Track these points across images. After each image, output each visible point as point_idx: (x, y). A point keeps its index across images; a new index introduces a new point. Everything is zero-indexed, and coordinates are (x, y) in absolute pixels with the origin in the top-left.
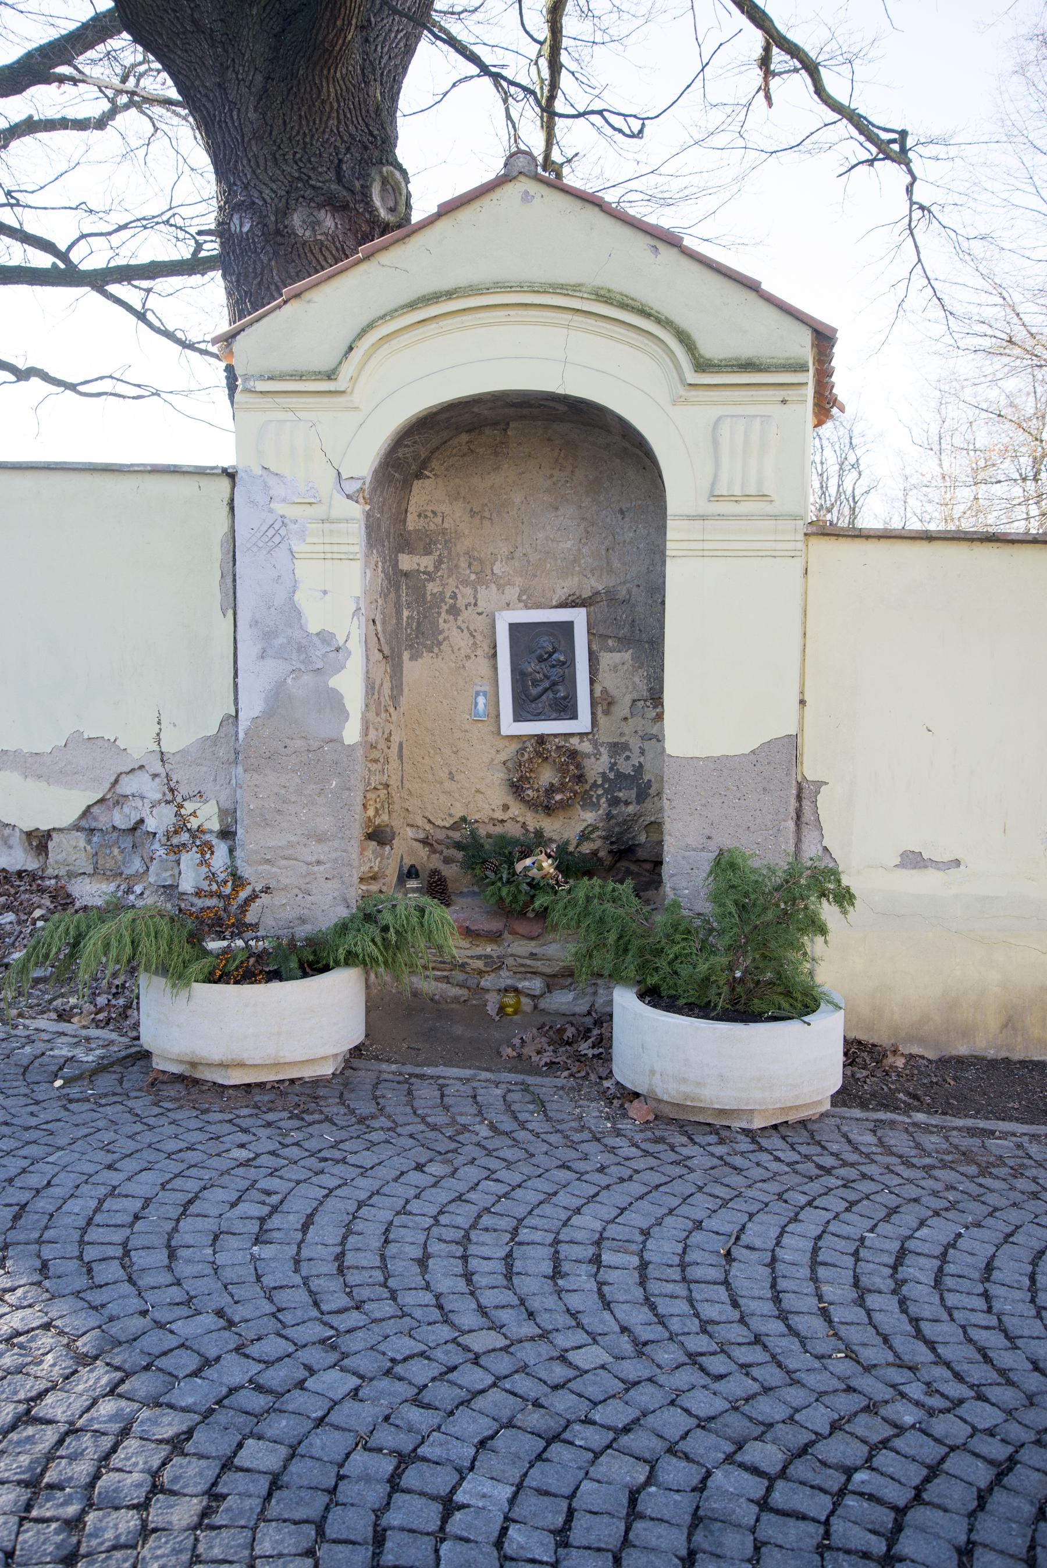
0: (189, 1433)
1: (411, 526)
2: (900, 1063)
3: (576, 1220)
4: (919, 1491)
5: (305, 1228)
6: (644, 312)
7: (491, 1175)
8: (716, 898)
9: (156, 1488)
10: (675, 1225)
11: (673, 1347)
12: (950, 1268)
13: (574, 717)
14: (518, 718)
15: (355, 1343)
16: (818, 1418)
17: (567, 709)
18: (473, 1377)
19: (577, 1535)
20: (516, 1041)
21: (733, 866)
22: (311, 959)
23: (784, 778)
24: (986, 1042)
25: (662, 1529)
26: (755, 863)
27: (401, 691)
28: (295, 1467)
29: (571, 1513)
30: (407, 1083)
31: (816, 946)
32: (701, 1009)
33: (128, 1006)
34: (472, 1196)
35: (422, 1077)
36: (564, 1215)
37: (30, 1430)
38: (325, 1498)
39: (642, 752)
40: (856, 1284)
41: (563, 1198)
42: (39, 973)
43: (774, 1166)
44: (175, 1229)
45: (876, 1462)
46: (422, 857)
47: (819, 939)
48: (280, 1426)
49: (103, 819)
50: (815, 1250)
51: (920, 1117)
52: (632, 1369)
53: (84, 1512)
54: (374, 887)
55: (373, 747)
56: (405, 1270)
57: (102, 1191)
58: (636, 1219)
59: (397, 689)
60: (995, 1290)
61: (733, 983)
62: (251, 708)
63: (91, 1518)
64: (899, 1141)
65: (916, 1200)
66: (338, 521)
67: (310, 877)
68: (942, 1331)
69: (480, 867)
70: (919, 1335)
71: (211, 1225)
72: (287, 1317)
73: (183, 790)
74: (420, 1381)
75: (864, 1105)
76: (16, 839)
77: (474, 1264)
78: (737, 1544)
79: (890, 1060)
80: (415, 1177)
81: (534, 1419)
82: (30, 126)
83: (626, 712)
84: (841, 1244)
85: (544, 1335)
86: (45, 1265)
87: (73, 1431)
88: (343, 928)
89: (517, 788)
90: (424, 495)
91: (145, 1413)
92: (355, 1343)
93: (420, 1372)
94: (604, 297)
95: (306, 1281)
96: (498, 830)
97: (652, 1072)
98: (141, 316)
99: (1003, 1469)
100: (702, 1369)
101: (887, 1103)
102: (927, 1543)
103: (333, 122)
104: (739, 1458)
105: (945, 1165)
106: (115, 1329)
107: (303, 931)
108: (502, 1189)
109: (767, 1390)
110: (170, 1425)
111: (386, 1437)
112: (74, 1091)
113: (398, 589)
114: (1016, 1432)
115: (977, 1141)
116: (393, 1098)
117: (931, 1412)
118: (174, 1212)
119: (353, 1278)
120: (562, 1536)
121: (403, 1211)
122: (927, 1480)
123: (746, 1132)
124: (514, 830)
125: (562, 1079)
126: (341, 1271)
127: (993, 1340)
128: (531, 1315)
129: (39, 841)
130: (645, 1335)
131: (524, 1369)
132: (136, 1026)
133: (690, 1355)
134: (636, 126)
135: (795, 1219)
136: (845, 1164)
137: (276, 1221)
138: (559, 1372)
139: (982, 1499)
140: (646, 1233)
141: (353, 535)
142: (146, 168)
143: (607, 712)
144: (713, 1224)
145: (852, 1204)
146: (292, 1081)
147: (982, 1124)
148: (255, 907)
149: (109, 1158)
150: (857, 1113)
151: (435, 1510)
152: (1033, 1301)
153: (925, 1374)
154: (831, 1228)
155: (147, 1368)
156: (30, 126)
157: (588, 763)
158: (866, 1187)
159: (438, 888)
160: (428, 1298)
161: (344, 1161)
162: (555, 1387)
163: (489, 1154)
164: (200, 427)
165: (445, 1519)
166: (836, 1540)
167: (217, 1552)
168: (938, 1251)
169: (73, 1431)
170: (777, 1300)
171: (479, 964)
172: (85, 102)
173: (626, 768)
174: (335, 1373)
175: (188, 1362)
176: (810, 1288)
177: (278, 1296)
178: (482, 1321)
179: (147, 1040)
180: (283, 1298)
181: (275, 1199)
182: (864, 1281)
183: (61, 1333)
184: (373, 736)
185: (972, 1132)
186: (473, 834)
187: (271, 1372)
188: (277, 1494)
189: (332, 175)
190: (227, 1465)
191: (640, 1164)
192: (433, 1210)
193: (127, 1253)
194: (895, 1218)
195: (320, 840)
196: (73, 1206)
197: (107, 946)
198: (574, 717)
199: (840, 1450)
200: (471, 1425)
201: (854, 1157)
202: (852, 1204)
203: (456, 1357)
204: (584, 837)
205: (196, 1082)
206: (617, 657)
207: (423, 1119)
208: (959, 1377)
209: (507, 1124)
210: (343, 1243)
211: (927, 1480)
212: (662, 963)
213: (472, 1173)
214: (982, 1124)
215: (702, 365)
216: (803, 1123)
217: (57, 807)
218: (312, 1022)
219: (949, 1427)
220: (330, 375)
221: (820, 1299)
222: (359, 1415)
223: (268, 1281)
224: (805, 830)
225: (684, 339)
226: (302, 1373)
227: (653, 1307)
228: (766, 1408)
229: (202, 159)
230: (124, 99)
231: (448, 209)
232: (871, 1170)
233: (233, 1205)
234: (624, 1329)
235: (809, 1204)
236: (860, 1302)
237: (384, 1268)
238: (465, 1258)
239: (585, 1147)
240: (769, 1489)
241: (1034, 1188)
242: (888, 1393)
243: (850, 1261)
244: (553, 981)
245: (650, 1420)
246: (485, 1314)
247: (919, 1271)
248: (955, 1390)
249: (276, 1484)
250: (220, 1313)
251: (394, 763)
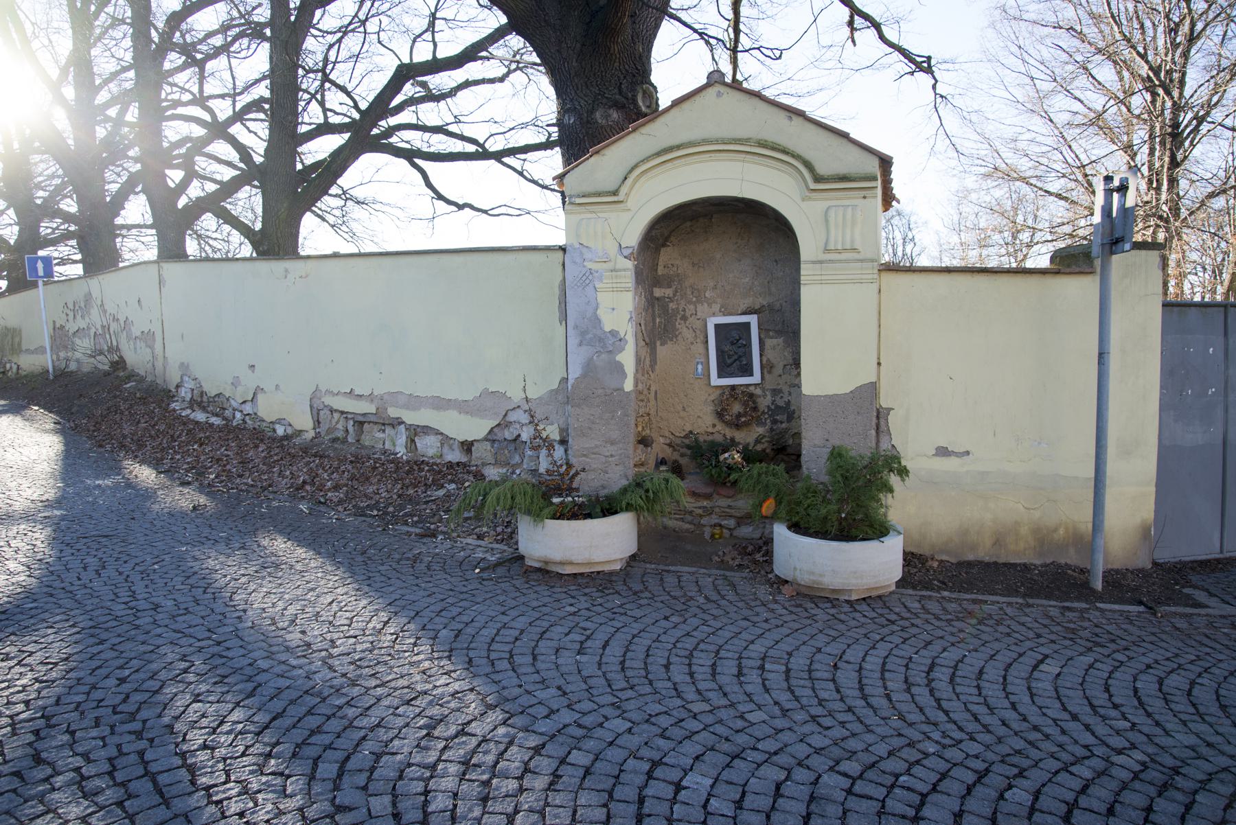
0: (543, 745)
1: (660, 273)
2: (935, 564)
3: (751, 647)
4: (935, 786)
5: (604, 647)
6: (785, 151)
7: (705, 623)
8: (830, 473)
9: (527, 770)
10: (806, 651)
11: (802, 712)
12: (959, 673)
13: (752, 375)
14: (720, 376)
15: (631, 705)
16: (882, 749)
17: (747, 371)
18: (694, 725)
19: (747, 803)
20: (721, 553)
21: (840, 455)
22: (606, 507)
23: (867, 404)
24: (984, 553)
25: (793, 803)
26: (853, 453)
27: (656, 363)
28: (598, 764)
29: (744, 793)
30: (660, 575)
31: (887, 499)
32: (822, 533)
33: (513, 532)
34: (694, 633)
35: (668, 571)
36: (745, 644)
37: (464, 739)
38: (614, 780)
39: (790, 394)
40: (906, 681)
41: (744, 635)
42: (466, 515)
43: (863, 620)
44: (536, 646)
45: (912, 771)
46: (668, 453)
47: (890, 495)
48: (590, 744)
49: (499, 435)
50: (884, 664)
51: (946, 594)
52: (779, 723)
53: (491, 779)
54: (642, 470)
55: (641, 393)
56: (657, 670)
57: (499, 625)
58: (785, 646)
59: (654, 361)
60: (983, 684)
61: (840, 520)
62: (575, 373)
63: (495, 781)
64: (933, 607)
65: (942, 638)
66: (620, 270)
67: (607, 462)
68: (954, 706)
69: (701, 458)
70: (940, 707)
71: (555, 644)
72: (594, 692)
73: (538, 416)
74: (664, 726)
75: (914, 588)
76: (456, 446)
77: (694, 668)
78: (834, 810)
79: (930, 563)
80: (664, 623)
81: (726, 747)
82: (467, 84)
83: (780, 372)
84: (899, 661)
85: (732, 705)
86: (470, 660)
87: (485, 740)
88: (624, 491)
89: (720, 415)
90: (668, 256)
91: (521, 735)
92: (631, 705)
93: (664, 721)
94: (763, 144)
95: (604, 674)
96: (710, 438)
97: (795, 569)
98: (521, 174)
99: (981, 776)
100: (819, 724)
101: (927, 586)
102: (938, 813)
103: (617, 64)
104: (837, 768)
105: (958, 619)
106: (505, 693)
107: (603, 493)
108: (711, 630)
109: (854, 735)
110: (533, 741)
111: (646, 752)
112: (485, 575)
113: (653, 307)
114: (990, 756)
115: (977, 606)
116: (652, 582)
117: (944, 747)
118: (536, 637)
119: (629, 673)
120: (739, 804)
121: (657, 640)
122: (940, 780)
123: (847, 602)
124: (718, 438)
125: (746, 573)
126: (623, 669)
127: (981, 710)
128: (725, 694)
129: (467, 446)
130: (787, 706)
131: (720, 722)
132: (517, 543)
133: (812, 717)
134: (777, 53)
135: (873, 648)
136: (903, 618)
137: (589, 643)
138: (740, 724)
139: (969, 790)
140: (790, 654)
141: (629, 279)
142: (524, 99)
143: (770, 372)
144: (828, 649)
145: (906, 640)
146: (598, 573)
147: (980, 597)
148: (578, 479)
149: (503, 609)
150: (911, 592)
151: (671, 788)
152: (1004, 690)
153: (942, 727)
154: (894, 652)
155: (522, 713)
156: (467, 84)
157: (760, 400)
158: (914, 630)
159: (677, 470)
160: (669, 685)
161: (625, 614)
162: (737, 731)
163: (704, 612)
164: (547, 224)
165: (676, 794)
166: (888, 809)
167: (557, 802)
168: (953, 664)
169: (485, 740)
170: (861, 689)
171: (700, 511)
172: (491, 69)
173: (781, 403)
174: (619, 720)
175: (544, 711)
176: (880, 683)
177: (590, 681)
178: (699, 697)
179: (523, 549)
180: (592, 682)
181: (588, 632)
182: (911, 680)
183: (479, 693)
184: (640, 387)
185: (974, 601)
186: (696, 440)
187: (585, 718)
188: (588, 777)
189: (616, 91)
190: (563, 761)
191: (788, 618)
192: (673, 640)
193: (512, 656)
194: (929, 647)
195: (612, 444)
196: (484, 632)
197: (498, 499)
198: (752, 375)
199: (892, 765)
200: (691, 748)
201: (908, 615)
202: (906, 640)
203: (684, 714)
204: (758, 441)
205: (548, 572)
206: (775, 341)
207: (669, 593)
208: (960, 729)
209: (714, 597)
210: (624, 656)
211: (940, 780)
212: (801, 509)
213: (695, 622)
214: (980, 597)
215: (818, 179)
216: (880, 597)
217: (475, 428)
218: (607, 541)
219: (954, 754)
220: (615, 193)
221: (886, 689)
222: (633, 741)
223: (585, 673)
224: (881, 436)
225: (808, 165)
226: (602, 719)
227: (792, 692)
228: (853, 744)
229: (551, 92)
230: (514, 66)
231: (676, 103)
232: (917, 621)
233: (567, 635)
234: (776, 703)
235: (882, 639)
236: (908, 690)
237: (646, 669)
238: (690, 665)
239: (757, 609)
240: (853, 784)
241: (1008, 630)
242: (921, 737)
243: (903, 669)
244: (742, 520)
245: (789, 748)
246: (700, 694)
247: (942, 675)
248: (958, 735)
249: (587, 772)
250: (559, 688)
251: (653, 402)
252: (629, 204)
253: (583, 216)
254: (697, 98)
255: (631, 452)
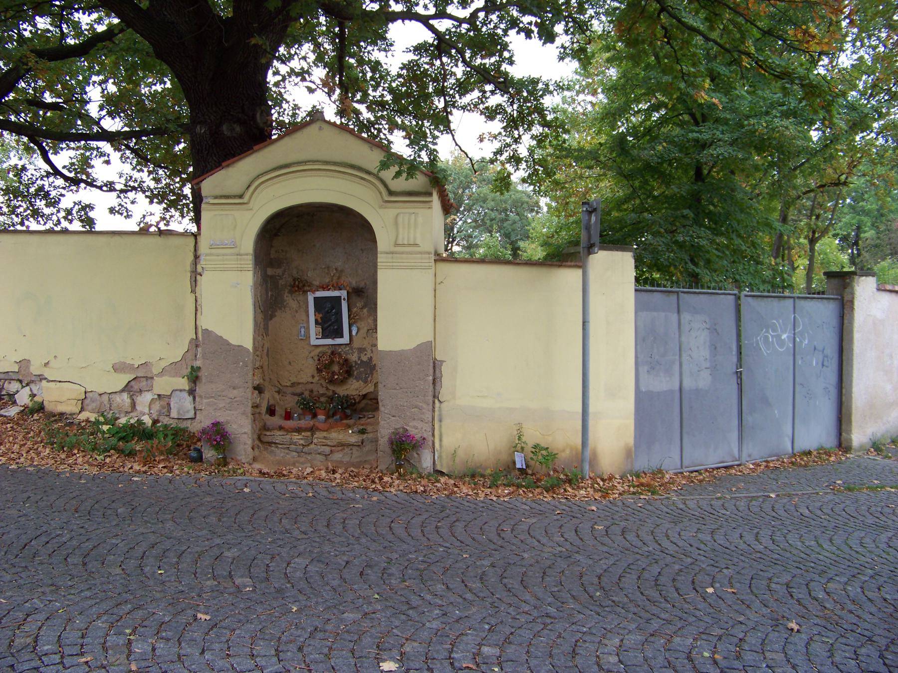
94: (353, 167)
173: (365, 359)
195: (234, 388)
198: (342, 337)
215: (391, 193)
252: (251, 205)
253: (217, 213)
254: (125, 237)
255: (250, 395)
